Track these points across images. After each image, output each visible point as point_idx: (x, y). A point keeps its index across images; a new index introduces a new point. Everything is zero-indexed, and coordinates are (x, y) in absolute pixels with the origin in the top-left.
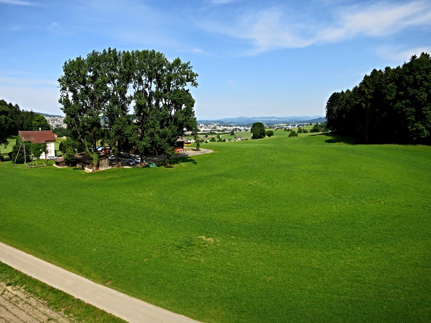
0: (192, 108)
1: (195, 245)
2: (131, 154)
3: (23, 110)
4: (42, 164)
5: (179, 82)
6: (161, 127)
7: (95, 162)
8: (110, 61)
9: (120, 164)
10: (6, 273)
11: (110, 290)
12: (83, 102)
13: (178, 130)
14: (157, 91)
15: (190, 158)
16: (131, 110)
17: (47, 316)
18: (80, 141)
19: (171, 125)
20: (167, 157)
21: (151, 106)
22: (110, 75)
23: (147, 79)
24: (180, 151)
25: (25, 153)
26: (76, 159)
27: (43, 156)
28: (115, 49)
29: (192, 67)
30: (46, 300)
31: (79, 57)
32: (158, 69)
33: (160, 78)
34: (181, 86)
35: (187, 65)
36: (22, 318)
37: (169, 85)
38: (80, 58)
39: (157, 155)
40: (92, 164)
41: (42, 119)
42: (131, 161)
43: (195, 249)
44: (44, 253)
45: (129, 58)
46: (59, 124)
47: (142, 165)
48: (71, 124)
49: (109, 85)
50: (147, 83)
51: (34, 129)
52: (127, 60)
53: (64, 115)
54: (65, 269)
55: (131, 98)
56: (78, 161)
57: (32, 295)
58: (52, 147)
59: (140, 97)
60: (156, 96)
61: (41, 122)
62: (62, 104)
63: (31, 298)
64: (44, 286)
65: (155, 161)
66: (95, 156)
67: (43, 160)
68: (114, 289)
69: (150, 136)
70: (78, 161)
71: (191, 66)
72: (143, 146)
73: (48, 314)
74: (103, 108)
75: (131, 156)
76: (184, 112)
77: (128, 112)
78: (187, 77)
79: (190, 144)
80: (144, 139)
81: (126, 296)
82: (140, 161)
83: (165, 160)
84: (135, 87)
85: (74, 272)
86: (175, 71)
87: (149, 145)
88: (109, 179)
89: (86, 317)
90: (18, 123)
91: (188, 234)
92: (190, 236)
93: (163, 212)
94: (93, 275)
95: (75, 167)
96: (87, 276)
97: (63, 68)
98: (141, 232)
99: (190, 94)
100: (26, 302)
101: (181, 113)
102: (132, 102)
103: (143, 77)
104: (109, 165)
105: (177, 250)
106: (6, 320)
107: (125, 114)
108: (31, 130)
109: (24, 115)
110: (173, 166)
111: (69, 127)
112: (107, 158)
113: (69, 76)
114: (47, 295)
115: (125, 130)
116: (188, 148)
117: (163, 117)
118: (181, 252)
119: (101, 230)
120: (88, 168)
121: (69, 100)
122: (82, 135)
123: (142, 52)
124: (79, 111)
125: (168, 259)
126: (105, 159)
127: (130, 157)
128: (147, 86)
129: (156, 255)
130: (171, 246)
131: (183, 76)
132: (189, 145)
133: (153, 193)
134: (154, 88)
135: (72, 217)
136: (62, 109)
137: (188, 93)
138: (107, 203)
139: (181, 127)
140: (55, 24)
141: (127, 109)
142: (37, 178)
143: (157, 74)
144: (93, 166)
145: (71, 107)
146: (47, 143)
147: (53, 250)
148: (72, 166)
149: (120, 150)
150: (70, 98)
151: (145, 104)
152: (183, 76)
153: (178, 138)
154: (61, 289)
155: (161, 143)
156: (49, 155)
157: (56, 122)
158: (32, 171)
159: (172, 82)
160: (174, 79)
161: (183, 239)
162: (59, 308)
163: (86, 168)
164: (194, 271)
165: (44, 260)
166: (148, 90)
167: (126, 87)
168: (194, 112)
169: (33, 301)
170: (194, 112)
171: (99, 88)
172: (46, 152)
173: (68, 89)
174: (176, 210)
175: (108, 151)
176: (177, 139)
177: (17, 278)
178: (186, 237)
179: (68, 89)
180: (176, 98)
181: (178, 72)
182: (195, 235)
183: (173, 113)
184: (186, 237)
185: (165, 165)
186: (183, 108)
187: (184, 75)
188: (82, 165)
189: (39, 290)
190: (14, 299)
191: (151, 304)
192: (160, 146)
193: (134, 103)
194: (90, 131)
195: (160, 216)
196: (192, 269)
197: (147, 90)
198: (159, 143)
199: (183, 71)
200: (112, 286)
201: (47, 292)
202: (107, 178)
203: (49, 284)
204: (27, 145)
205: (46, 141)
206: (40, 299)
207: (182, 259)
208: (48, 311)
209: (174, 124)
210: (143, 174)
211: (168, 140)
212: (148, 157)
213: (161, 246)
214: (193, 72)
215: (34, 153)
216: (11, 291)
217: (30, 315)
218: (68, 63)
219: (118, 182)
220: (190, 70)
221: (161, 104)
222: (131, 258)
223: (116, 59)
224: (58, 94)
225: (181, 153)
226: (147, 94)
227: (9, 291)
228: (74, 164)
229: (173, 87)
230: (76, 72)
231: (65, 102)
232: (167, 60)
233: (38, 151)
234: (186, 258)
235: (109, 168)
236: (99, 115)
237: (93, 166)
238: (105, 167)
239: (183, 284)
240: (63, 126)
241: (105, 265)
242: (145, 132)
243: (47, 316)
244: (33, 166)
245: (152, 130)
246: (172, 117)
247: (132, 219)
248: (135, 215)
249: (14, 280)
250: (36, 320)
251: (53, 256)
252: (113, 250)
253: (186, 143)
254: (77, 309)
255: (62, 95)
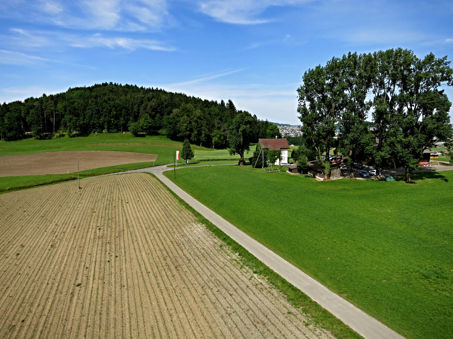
0: (448, 113)
1: (447, 278)
2: (364, 165)
3: (259, 120)
4: (276, 169)
5: (431, 82)
6: (405, 136)
7: (327, 171)
8: (349, 66)
9: (353, 174)
10: (253, 262)
11: (346, 302)
12: (320, 110)
13: (426, 140)
14: (402, 94)
15: (438, 173)
16: (370, 117)
17: (287, 309)
18: (314, 149)
19: (417, 133)
20: (409, 170)
21: (392, 112)
22: (348, 81)
23: (391, 82)
24: (425, 164)
25: (263, 158)
26: (308, 167)
27: (277, 163)
28: (356, 53)
29: (449, 62)
30: (286, 295)
31: (318, 65)
32: (405, 69)
33: (407, 80)
34: (433, 87)
35: (443, 61)
36: (266, 304)
37: (417, 86)
38: (320, 67)
39: (395, 168)
40: (324, 173)
41: (275, 128)
42: (364, 173)
43: (447, 283)
44: (282, 251)
45: (370, 61)
46: (287, 132)
47: (377, 178)
48: (306, 132)
49: (346, 92)
50: (389, 86)
51: (267, 137)
52: (368, 63)
53: (301, 124)
54: (302, 271)
55: (370, 104)
56: (309, 169)
57: (274, 287)
58: (285, 154)
59: (381, 103)
60: (400, 100)
61: (274, 130)
62: (300, 113)
63: (273, 289)
64: (284, 281)
65: (392, 175)
66: (327, 165)
67: (277, 166)
68: (351, 302)
69: (390, 146)
70: (309, 169)
71: (449, 61)
72: (381, 156)
73: (289, 307)
74: (339, 116)
75: (364, 167)
76: (436, 118)
77: (365, 119)
78: (442, 75)
79: (437, 157)
80: (382, 149)
81: (364, 314)
82: (375, 173)
83: (406, 174)
84: (375, 91)
85: (310, 276)
86: (426, 70)
87: (389, 156)
88: (341, 190)
89: (324, 322)
90: (255, 132)
91: (437, 264)
92: (440, 267)
93: (405, 233)
94: (328, 283)
95: (306, 175)
96: (323, 282)
97: (303, 78)
98: (377, 250)
99: (445, 96)
100: (269, 292)
101: (432, 119)
102: (371, 108)
103: (385, 80)
104: (341, 176)
105: (423, 279)
106: (253, 302)
107: (362, 122)
108: (265, 138)
109: (260, 124)
110: (416, 181)
111: (304, 135)
112: (340, 167)
113: (308, 85)
114: (287, 290)
115: (361, 139)
116: (435, 162)
117: (408, 124)
118: (428, 282)
119: (335, 240)
120: (320, 177)
121: (307, 110)
122: (317, 143)
123: (386, 52)
124: (315, 120)
125: (411, 286)
126: (337, 169)
127: (363, 168)
128: (389, 89)
129: (397, 279)
130: (415, 273)
131: (437, 75)
132: (436, 157)
133: (391, 210)
134: (397, 91)
135: (306, 223)
136: (299, 118)
137: (442, 95)
138: (340, 214)
139: (430, 135)
140: (288, 36)
141: (364, 116)
142: (274, 182)
143: (403, 74)
144: (324, 174)
145: (308, 116)
146: (282, 150)
147: (290, 251)
148: (304, 173)
149: (353, 160)
150: (308, 107)
151: (386, 110)
152: (437, 75)
153: (425, 148)
154: (299, 288)
155: (403, 154)
156: (282, 162)
157: (284, 131)
158: (269, 175)
159: (421, 84)
160: (424, 79)
161: (431, 267)
162: (297, 305)
163: (317, 177)
164: (446, 308)
165: (282, 257)
166: (391, 94)
167: (365, 93)
168: (449, 117)
169: (275, 292)
170: (449, 117)
171: (337, 95)
172: (281, 159)
173: (305, 98)
174: (422, 233)
175: (339, 161)
176: (423, 150)
177: (262, 268)
178: (434, 266)
179: (305, 98)
180: (427, 102)
181: (429, 70)
182: (448, 267)
183: (420, 119)
184: (434, 266)
185: (406, 180)
186: (434, 113)
187: (438, 73)
188: (313, 173)
189: (280, 284)
190: (259, 286)
191: (392, 330)
192: (401, 157)
193: (374, 109)
194: (325, 140)
195: (401, 237)
196: (444, 305)
197: (389, 94)
198: (401, 154)
199: (437, 69)
200: (348, 298)
201: (287, 287)
202: (338, 188)
203: (288, 281)
204: (265, 151)
205: (281, 149)
206: (281, 292)
207: (430, 290)
208: (288, 305)
209: (421, 132)
210: (379, 188)
211: (412, 151)
212: (384, 169)
213: (402, 270)
214: (450, 68)
215: (271, 159)
216: (257, 278)
217: (273, 304)
218: (308, 73)
219: (351, 193)
220: (446, 67)
221: (405, 109)
222: (368, 275)
223: (355, 63)
224: (296, 103)
225: (425, 167)
226: (389, 99)
227: (255, 278)
228: (305, 172)
229: (423, 89)
230: (315, 81)
231: (302, 110)
232: (417, 57)
233: (273, 157)
234: (436, 290)
235: (341, 178)
236: (335, 123)
237: (324, 174)
238: (336, 177)
239: (431, 319)
240: (291, 135)
241: (340, 276)
242: (383, 141)
243: (287, 309)
244: (269, 171)
245: (393, 139)
246: (418, 124)
247: (367, 234)
248: (370, 231)
249: (259, 270)
250: (278, 310)
251: (290, 256)
252: (348, 263)
253: (432, 155)
254: (314, 311)
255: (300, 104)
